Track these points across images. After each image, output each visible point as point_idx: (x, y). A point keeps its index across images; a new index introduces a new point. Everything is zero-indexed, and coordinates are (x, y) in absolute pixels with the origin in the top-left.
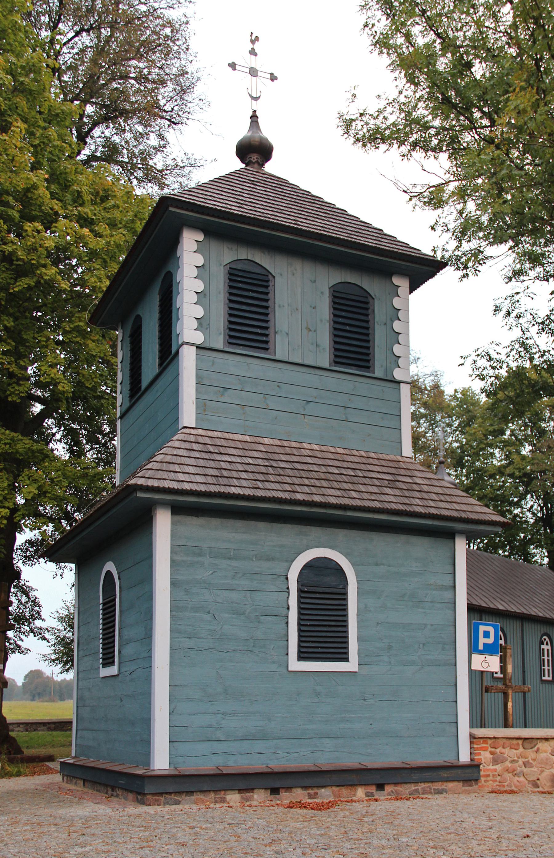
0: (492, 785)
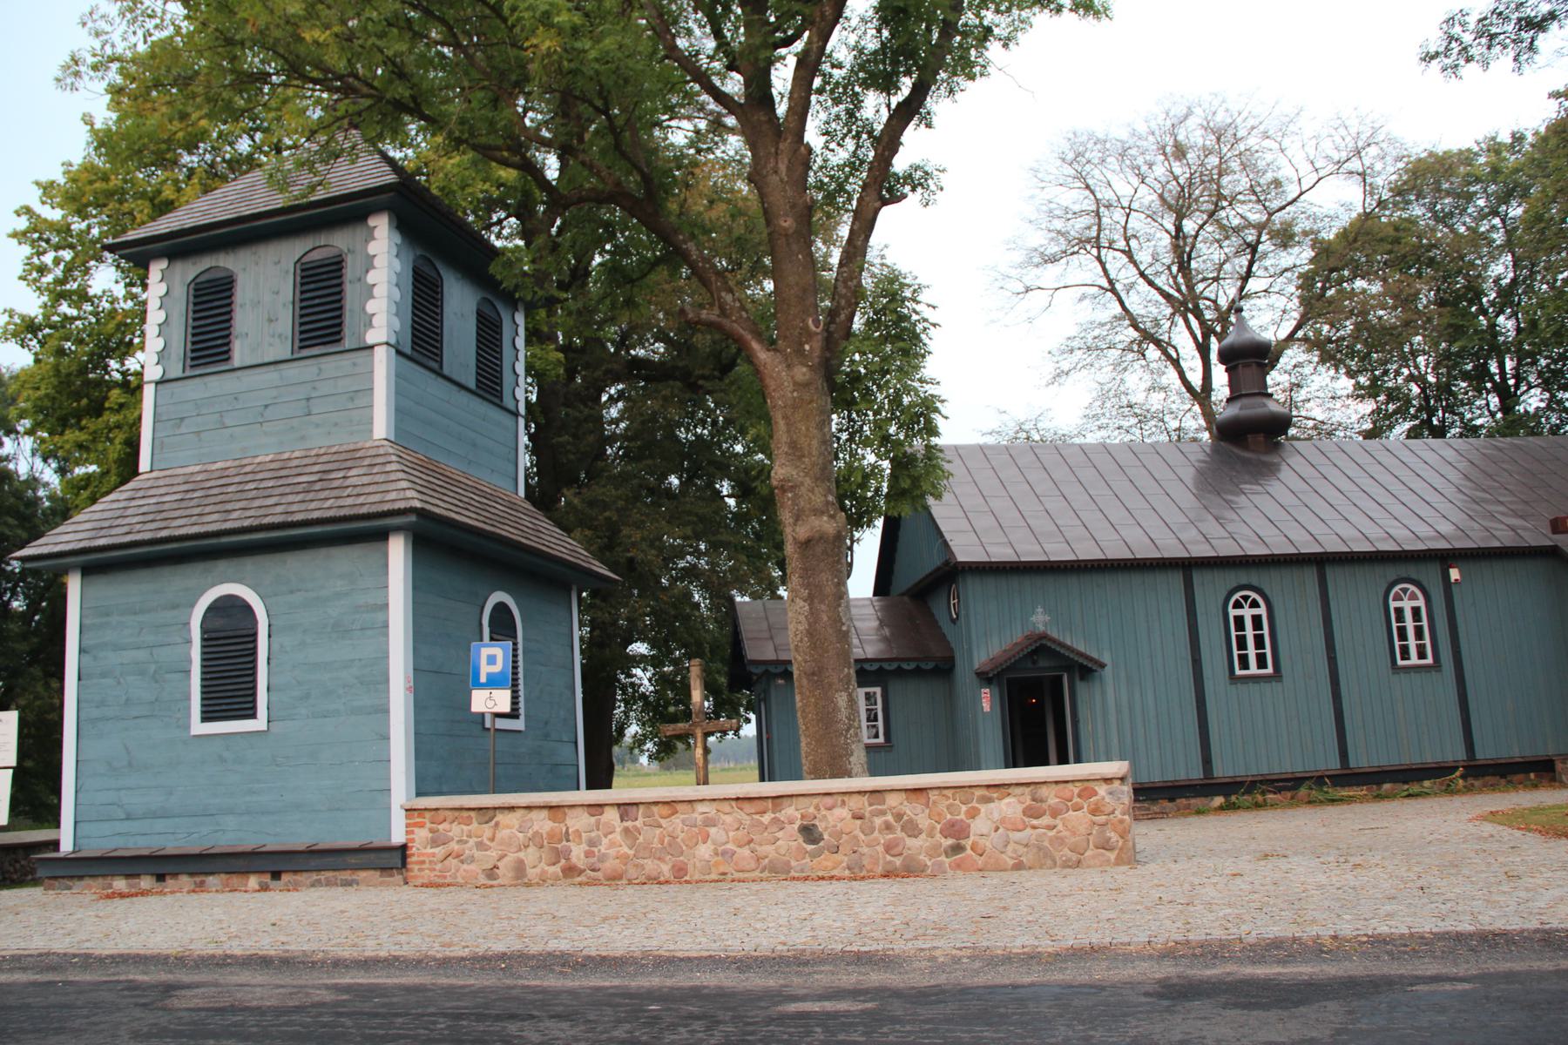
0: (427, 876)
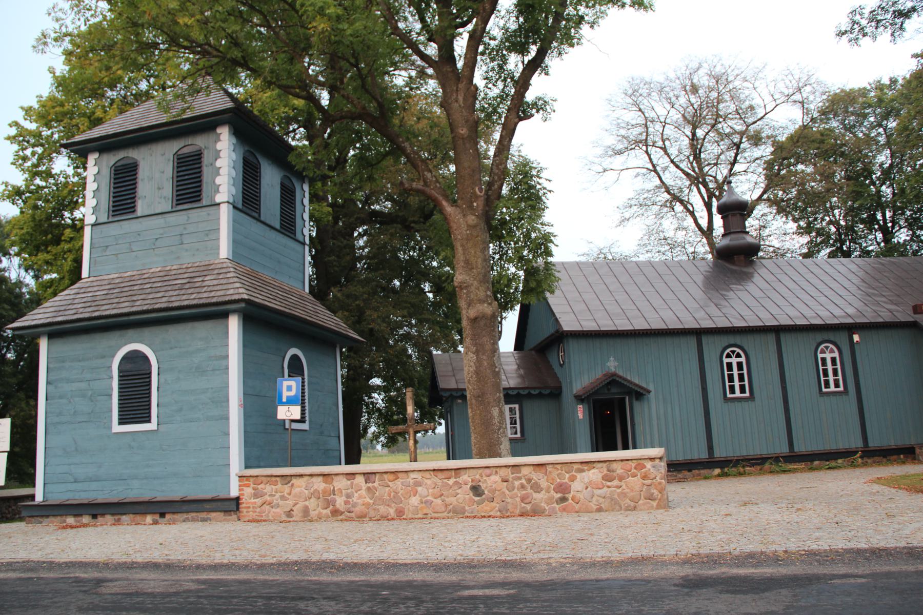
0: (252, 515)
